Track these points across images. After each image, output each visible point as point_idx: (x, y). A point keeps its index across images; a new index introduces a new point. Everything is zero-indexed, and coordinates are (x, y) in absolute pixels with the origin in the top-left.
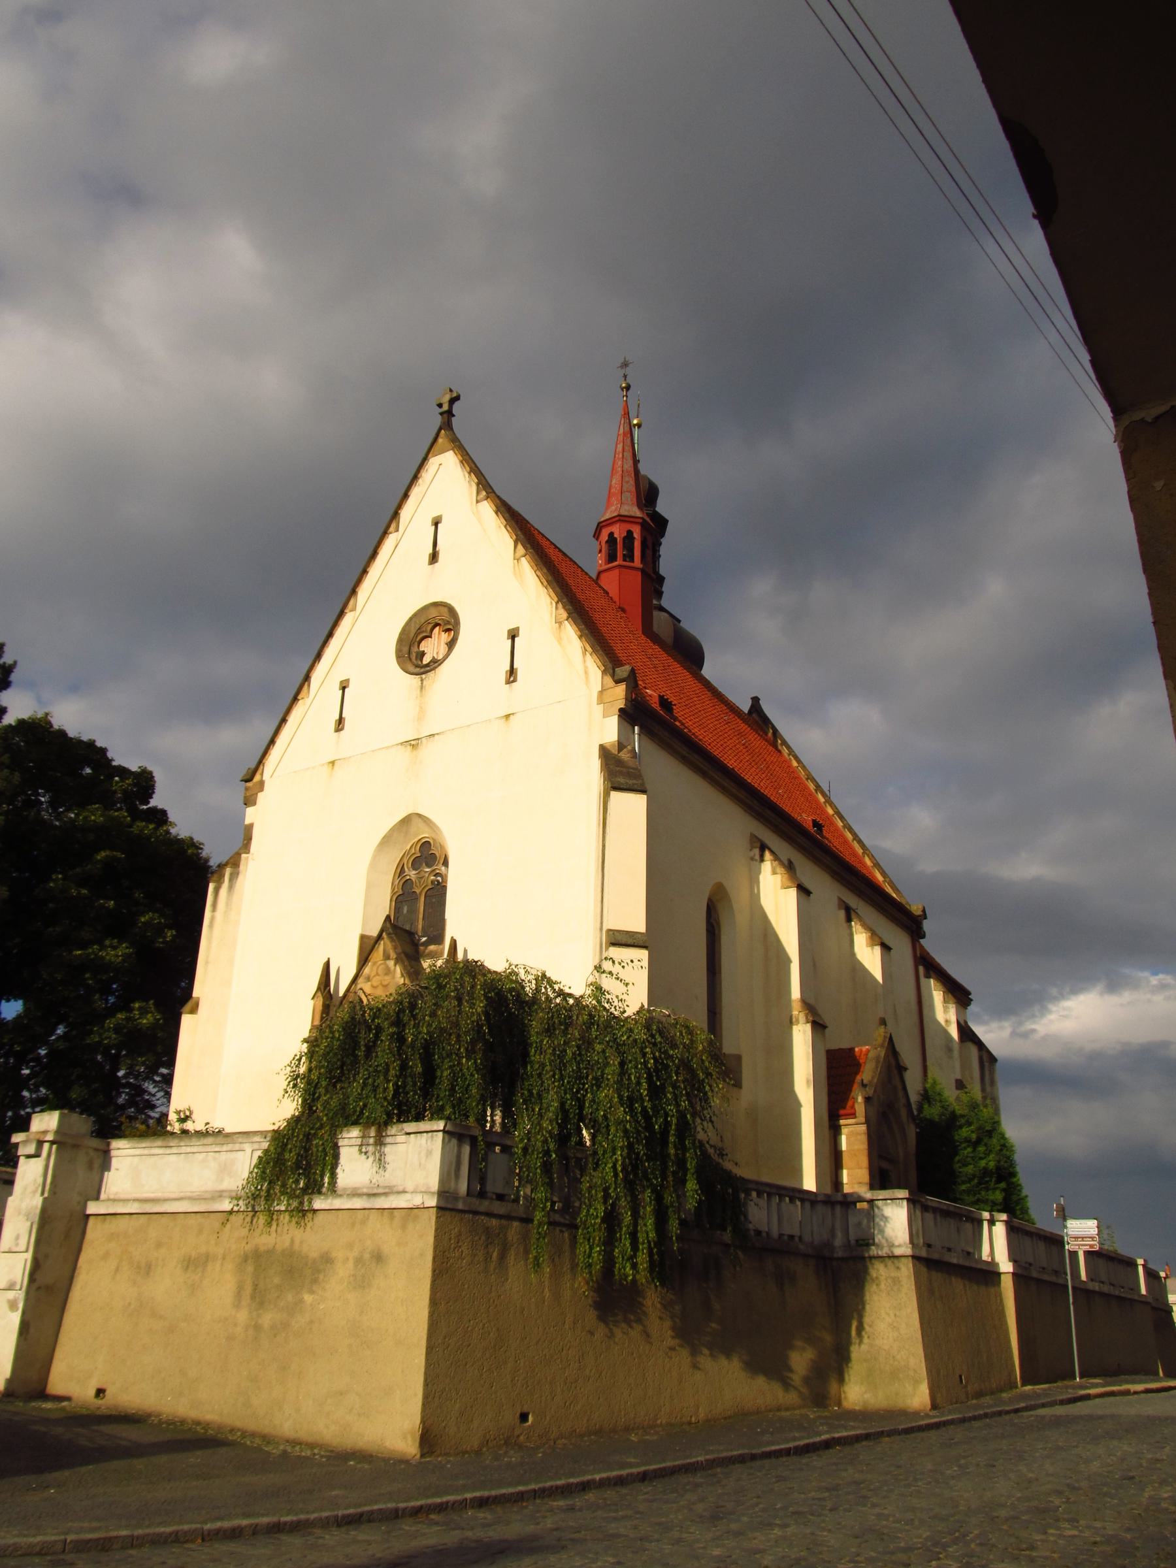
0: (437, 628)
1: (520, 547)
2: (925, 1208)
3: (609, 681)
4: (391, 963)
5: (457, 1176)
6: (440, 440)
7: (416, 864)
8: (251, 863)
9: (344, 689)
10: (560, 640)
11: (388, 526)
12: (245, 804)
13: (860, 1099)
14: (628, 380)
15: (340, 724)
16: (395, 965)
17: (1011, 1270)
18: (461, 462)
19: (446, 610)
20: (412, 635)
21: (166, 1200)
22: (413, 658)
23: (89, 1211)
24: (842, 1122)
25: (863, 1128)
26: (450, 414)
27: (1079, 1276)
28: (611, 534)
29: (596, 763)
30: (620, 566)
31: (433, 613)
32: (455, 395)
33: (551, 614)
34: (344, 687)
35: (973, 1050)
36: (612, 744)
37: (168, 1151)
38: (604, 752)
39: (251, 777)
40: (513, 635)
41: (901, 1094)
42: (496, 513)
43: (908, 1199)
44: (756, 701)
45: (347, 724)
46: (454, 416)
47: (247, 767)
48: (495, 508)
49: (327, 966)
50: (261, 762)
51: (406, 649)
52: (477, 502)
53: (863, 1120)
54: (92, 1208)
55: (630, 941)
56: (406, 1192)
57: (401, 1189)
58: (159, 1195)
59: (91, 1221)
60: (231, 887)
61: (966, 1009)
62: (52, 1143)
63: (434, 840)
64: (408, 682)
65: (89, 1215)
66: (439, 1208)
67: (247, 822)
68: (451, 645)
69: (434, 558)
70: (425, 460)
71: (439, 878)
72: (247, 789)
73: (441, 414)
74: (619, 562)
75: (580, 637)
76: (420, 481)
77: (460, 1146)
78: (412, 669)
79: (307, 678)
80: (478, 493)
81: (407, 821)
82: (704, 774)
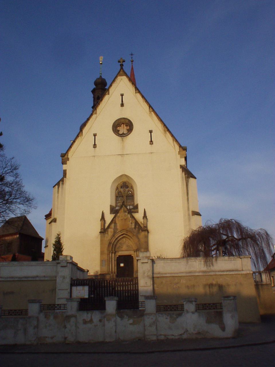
6: (121, 72)
8: (67, 181)
9: (151, 141)
10: (165, 136)
16: (128, 214)
19: (128, 120)
20: (116, 125)
26: (122, 65)
31: (123, 121)
37: (172, 261)
39: (64, 158)
40: (151, 132)
47: (61, 153)
49: (103, 212)
51: (114, 129)
60: (62, 187)
67: (64, 169)
70: (116, 77)
72: (62, 159)
76: (115, 82)
80: (135, 91)
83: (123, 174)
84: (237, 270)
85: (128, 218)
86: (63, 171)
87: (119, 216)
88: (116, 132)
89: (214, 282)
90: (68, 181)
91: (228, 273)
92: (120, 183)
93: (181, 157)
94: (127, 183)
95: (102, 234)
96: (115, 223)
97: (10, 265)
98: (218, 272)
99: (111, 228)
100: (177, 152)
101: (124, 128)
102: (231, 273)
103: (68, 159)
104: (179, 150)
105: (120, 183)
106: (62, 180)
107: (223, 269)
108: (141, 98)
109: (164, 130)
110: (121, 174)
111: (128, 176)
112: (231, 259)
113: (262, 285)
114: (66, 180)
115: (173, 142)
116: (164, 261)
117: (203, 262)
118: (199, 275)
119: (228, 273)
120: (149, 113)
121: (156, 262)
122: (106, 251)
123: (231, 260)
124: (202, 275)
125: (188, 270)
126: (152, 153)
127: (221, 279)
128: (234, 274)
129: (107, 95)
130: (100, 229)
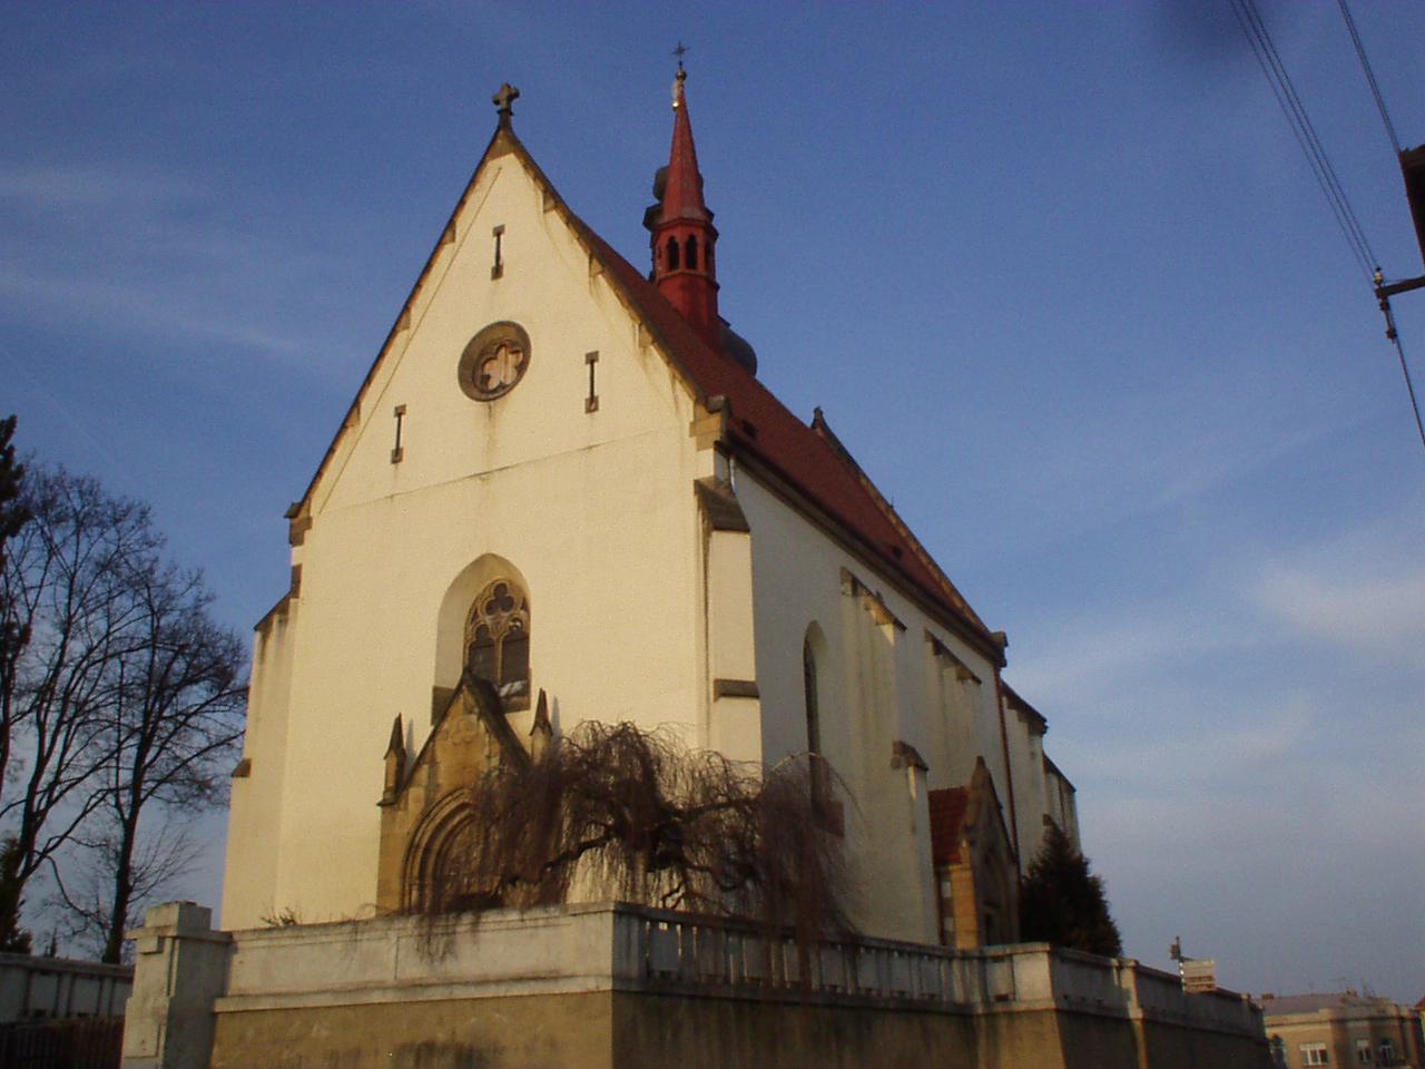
0: (503, 351)
1: (595, 261)
2: (1064, 960)
3: (702, 410)
4: (474, 717)
5: (628, 955)
6: (499, 141)
7: (490, 609)
10: (645, 366)
11: (443, 236)
12: (291, 542)
13: (964, 844)
14: (684, 68)
15: (397, 456)
16: (478, 719)
17: (1140, 1015)
18: (524, 166)
20: (475, 357)
21: (302, 994)
22: (478, 383)
23: (217, 1009)
24: (951, 868)
25: (968, 874)
26: (506, 114)
27: (16, 873)
28: (672, 239)
29: (691, 501)
30: (682, 274)
31: (499, 334)
32: (513, 92)
33: (634, 338)
34: (400, 412)
35: (1055, 780)
36: (708, 479)
37: (300, 941)
38: (700, 487)
39: (298, 519)
40: (592, 359)
41: (1002, 838)
42: (567, 224)
43: (1049, 953)
44: (818, 412)
45: (405, 455)
46: (511, 114)
48: (565, 219)
49: (398, 723)
50: (307, 496)
51: (469, 373)
52: (545, 211)
53: (968, 865)
54: (221, 1006)
55: (740, 691)
56: (577, 976)
57: (568, 972)
58: (294, 988)
59: (220, 1018)
60: (280, 636)
61: (1041, 736)
62: (174, 938)
63: (511, 583)
64: (470, 407)
65: (218, 1013)
66: (614, 991)
67: (294, 563)
68: (521, 368)
69: (497, 272)
70: (482, 163)
71: (518, 624)
72: (292, 526)
73: (499, 112)
74: (681, 268)
75: (668, 363)
76: (477, 187)
77: (629, 926)
78: (476, 393)
79: (356, 404)
80: (545, 202)
81: (481, 562)
82: (796, 506)
83: (484, 552)
84: (554, 976)
85: (477, 735)
86: (290, 570)
87: (447, 732)
88: (475, 386)
89: (441, 1036)
90: (304, 612)
91: (502, 991)
92: (481, 590)
93: (700, 447)
94: (508, 584)
95: (388, 810)
96: (433, 763)
97: (282, 943)
98: (380, 992)
99: (419, 785)
100: (687, 426)
101: (506, 362)
102: (517, 990)
103: (308, 523)
104: (695, 416)
105: (485, 590)
106: (282, 608)
107: (496, 970)
108: (564, 226)
109: (640, 341)
110: (476, 555)
111: (502, 558)
112: (537, 919)
113: (1012, 1015)
114: (296, 603)
115: (673, 384)
116: (271, 939)
117: (412, 943)
118: (384, 1001)
119: (502, 991)
120: (590, 283)
121: (240, 944)
122: (396, 885)
123: (536, 927)
124: (396, 1000)
125: (354, 976)
126: (590, 448)
127: (473, 1020)
128: (526, 993)
129: (446, 246)
130: (383, 789)
